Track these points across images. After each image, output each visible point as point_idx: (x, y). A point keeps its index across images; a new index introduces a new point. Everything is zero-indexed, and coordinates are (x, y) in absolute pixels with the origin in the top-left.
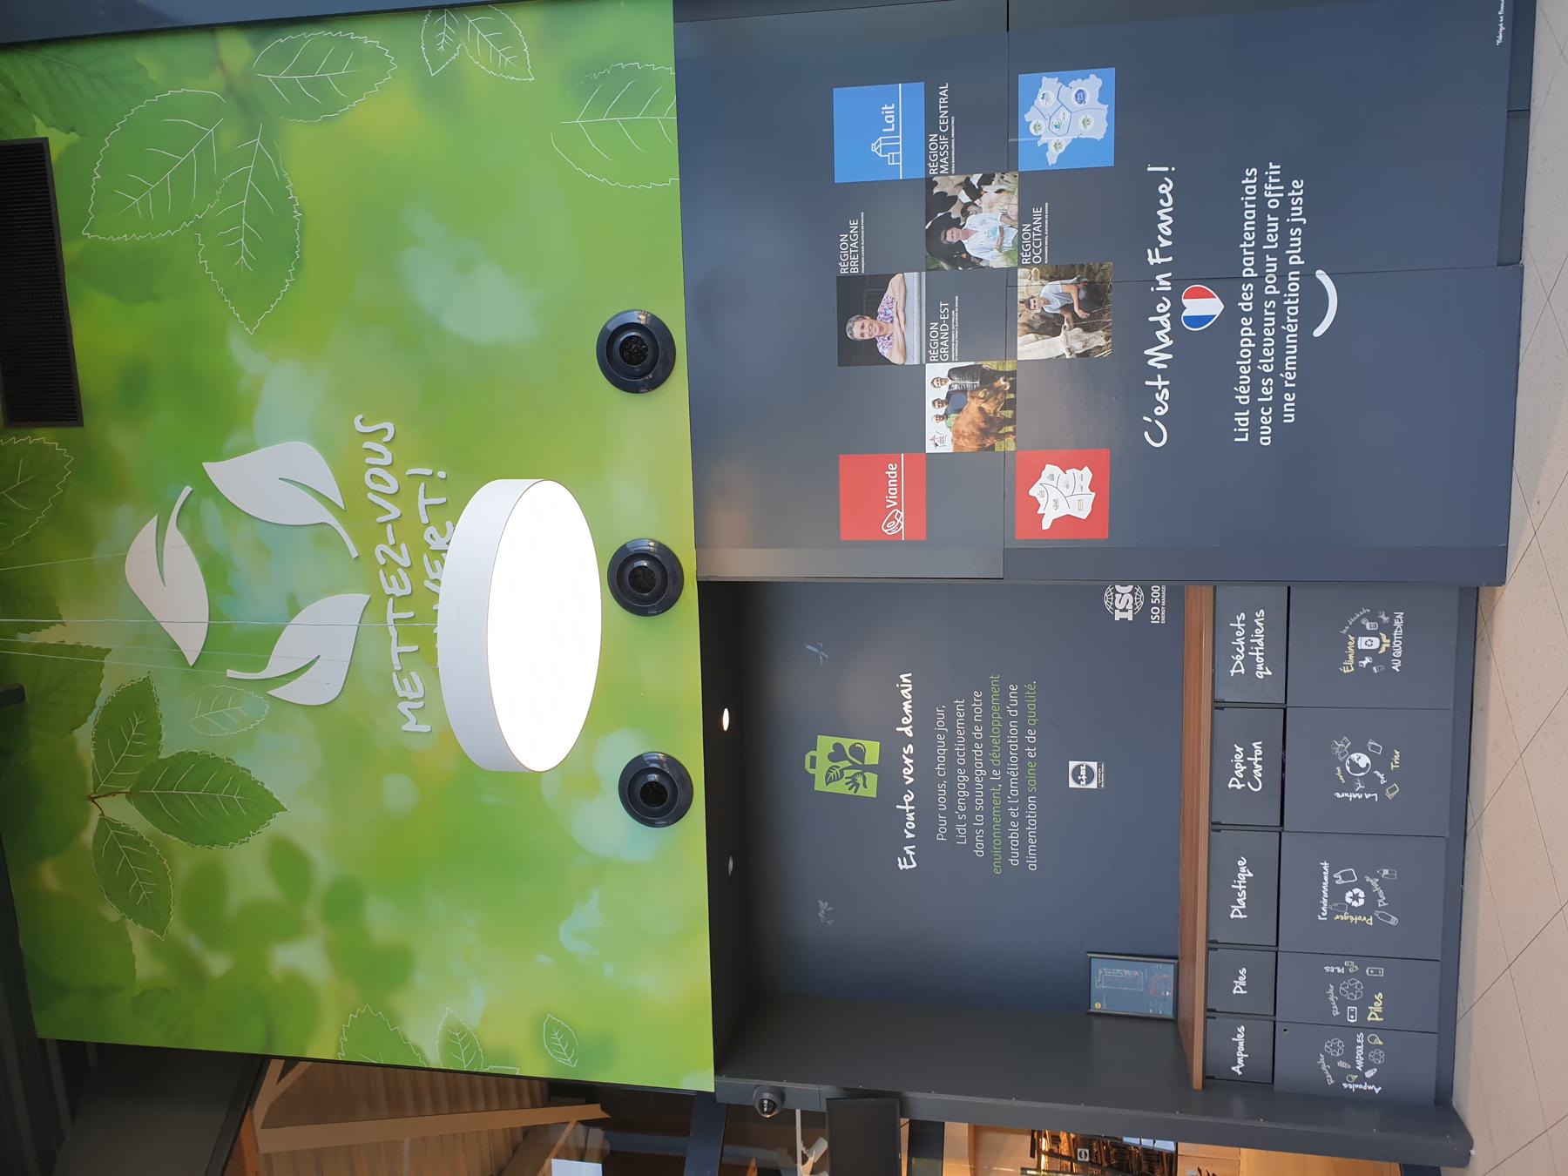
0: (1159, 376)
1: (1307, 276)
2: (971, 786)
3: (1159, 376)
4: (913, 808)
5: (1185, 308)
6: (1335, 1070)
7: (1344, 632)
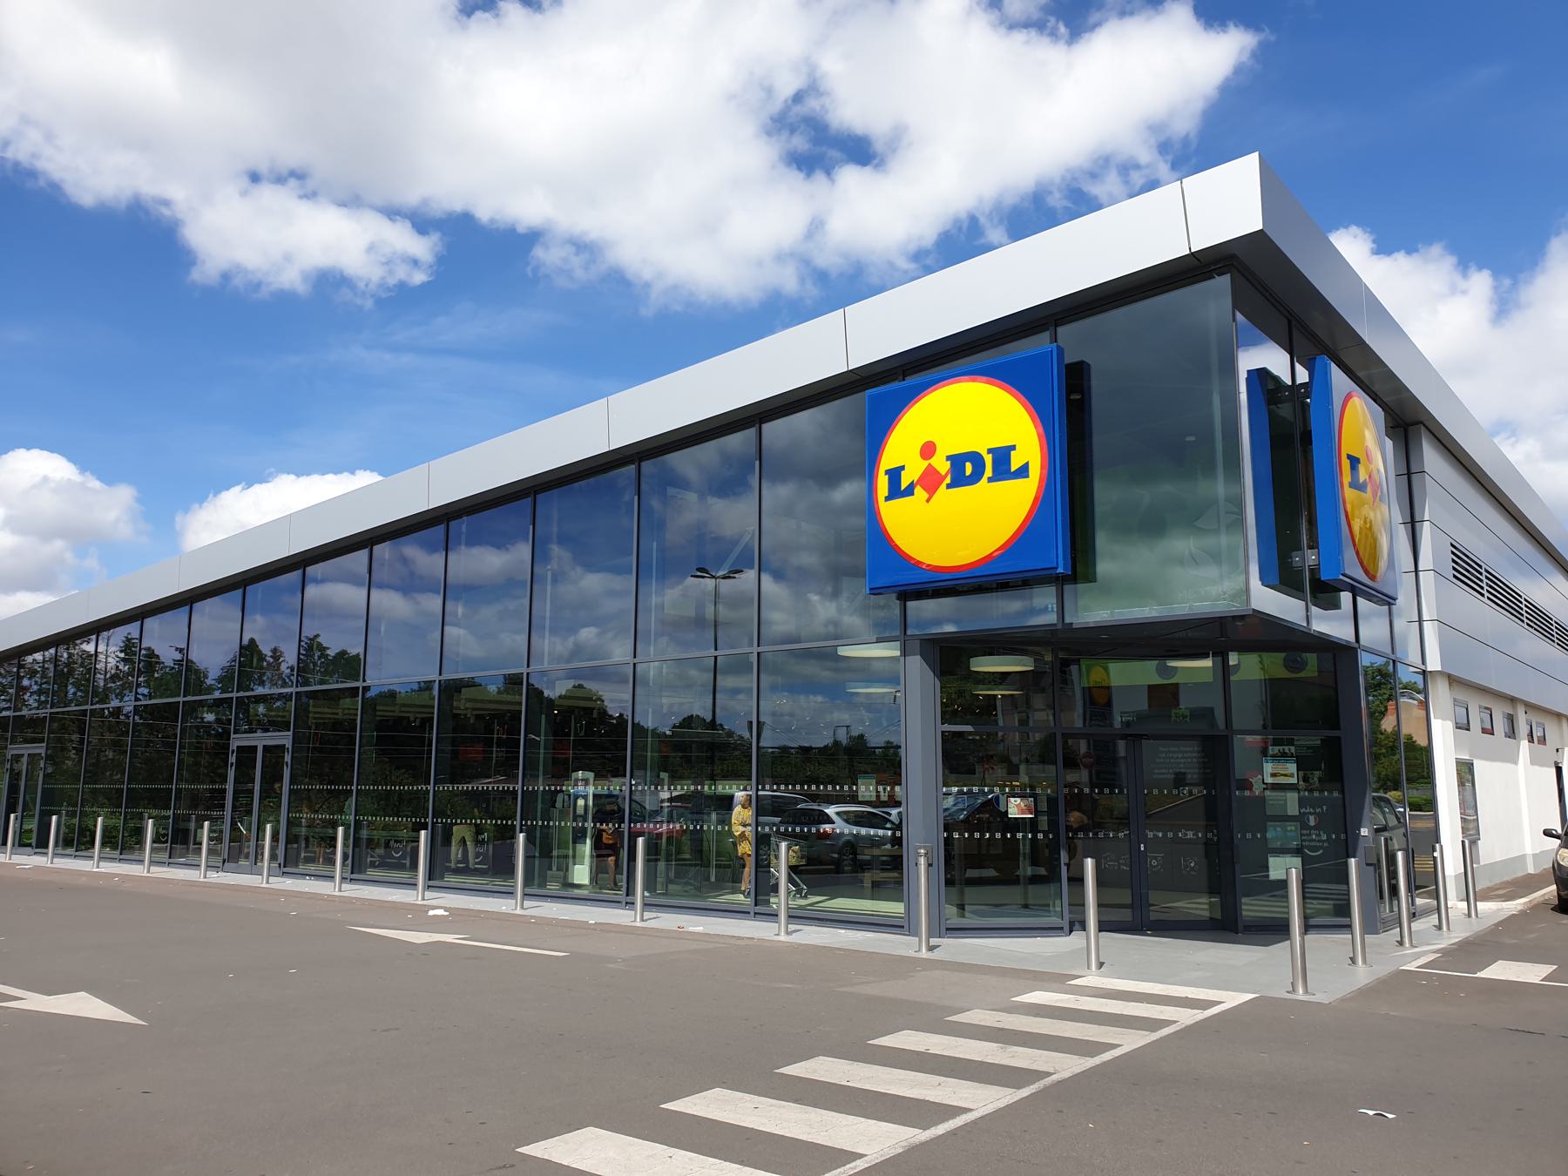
1: (1321, 847)
5: (1248, 371)
6: (1106, 857)
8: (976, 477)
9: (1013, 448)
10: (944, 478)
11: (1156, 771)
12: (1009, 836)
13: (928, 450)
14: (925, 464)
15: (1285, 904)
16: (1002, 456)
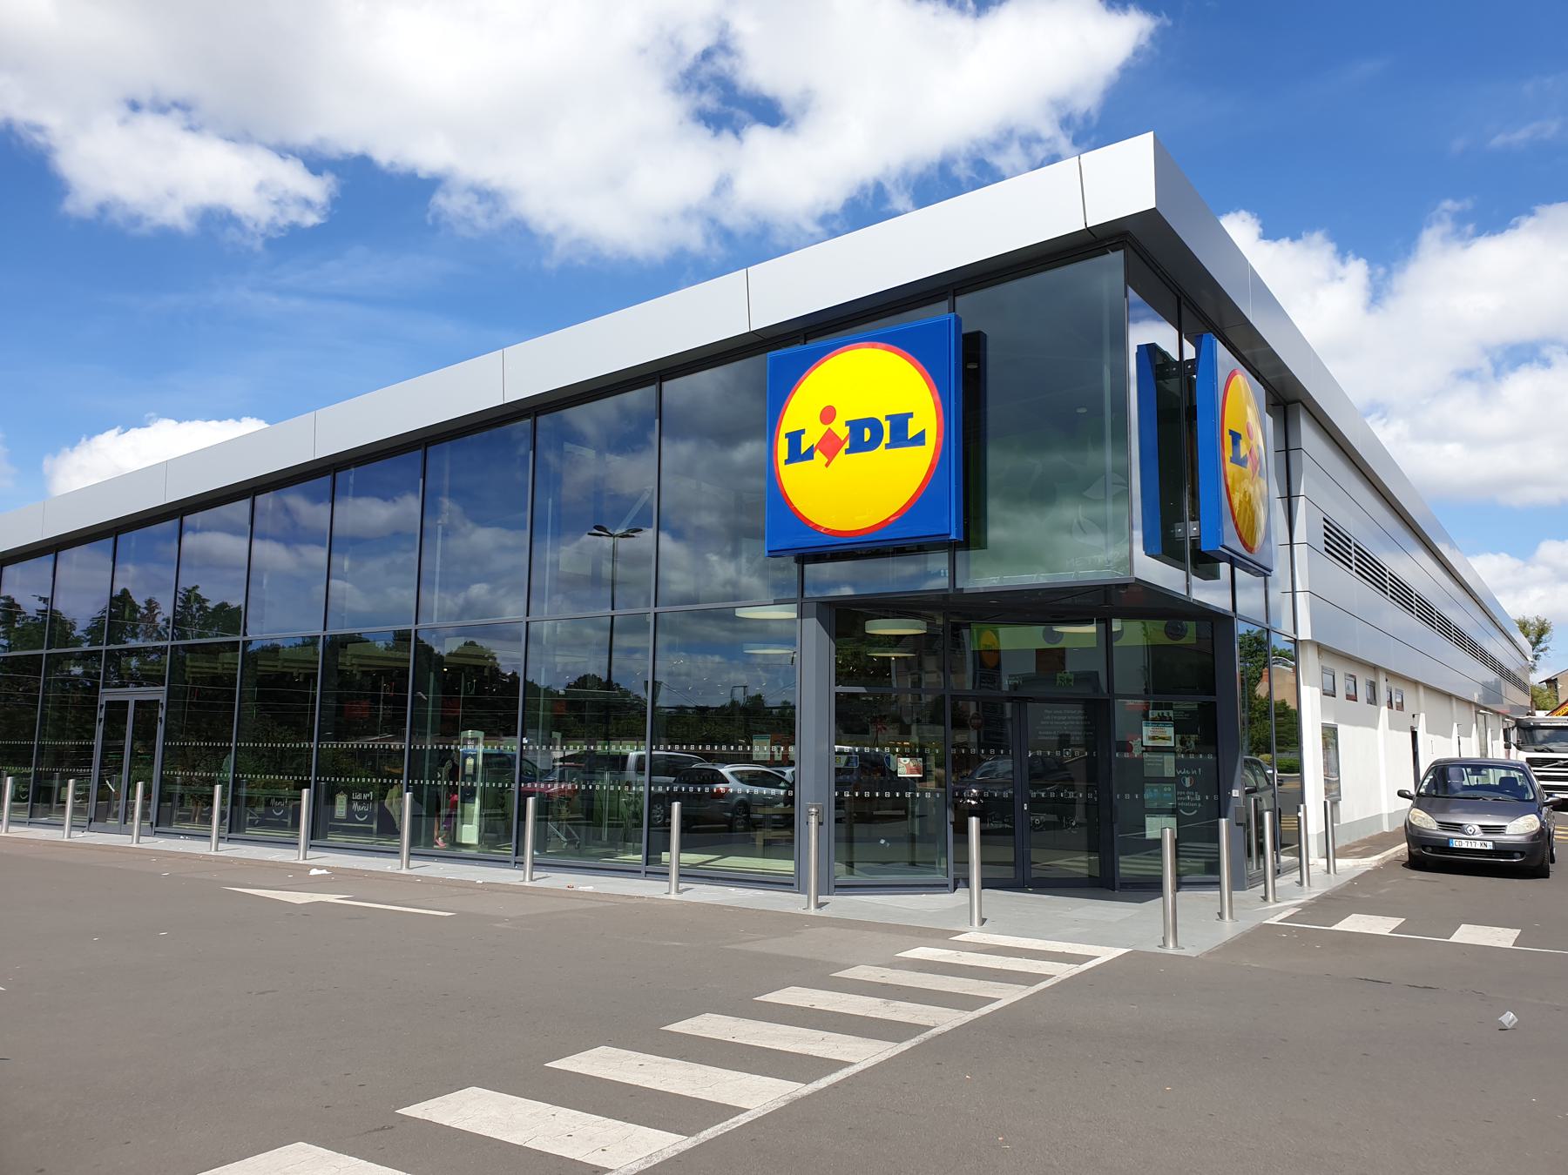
1: (1195, 808)
2: (1061, 720)
5: (1138, 346)
8: (874, 444)
11: (1040, 733)
13: (828, 415)
14: (824, 428)
16: (900, 423)
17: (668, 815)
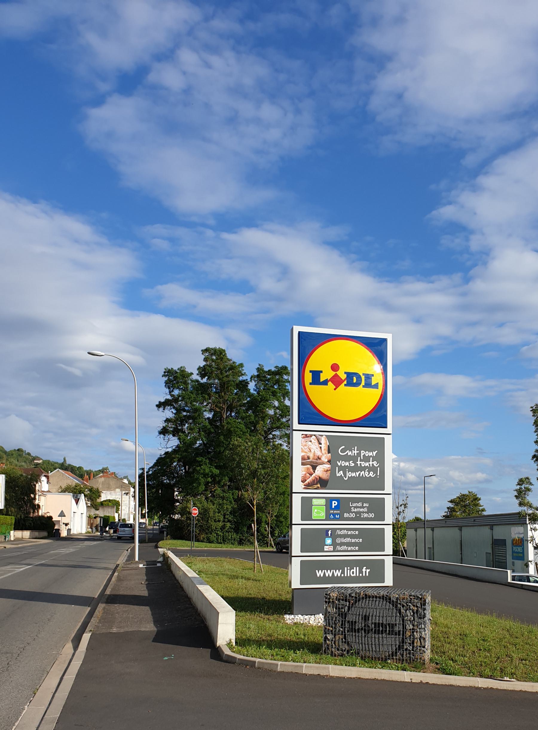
0: (358, 452)
3: (358, 452)
4: (371, 466)
7: (172, 658)
8: (357, 384)
9: (321, 372)
10: (343, 381)
12: (358, 515)
13: (335, 367)
14: (333, 373)
15: (505, 548)
17: (144, 531)
